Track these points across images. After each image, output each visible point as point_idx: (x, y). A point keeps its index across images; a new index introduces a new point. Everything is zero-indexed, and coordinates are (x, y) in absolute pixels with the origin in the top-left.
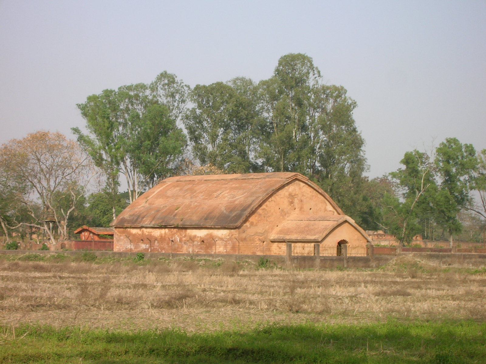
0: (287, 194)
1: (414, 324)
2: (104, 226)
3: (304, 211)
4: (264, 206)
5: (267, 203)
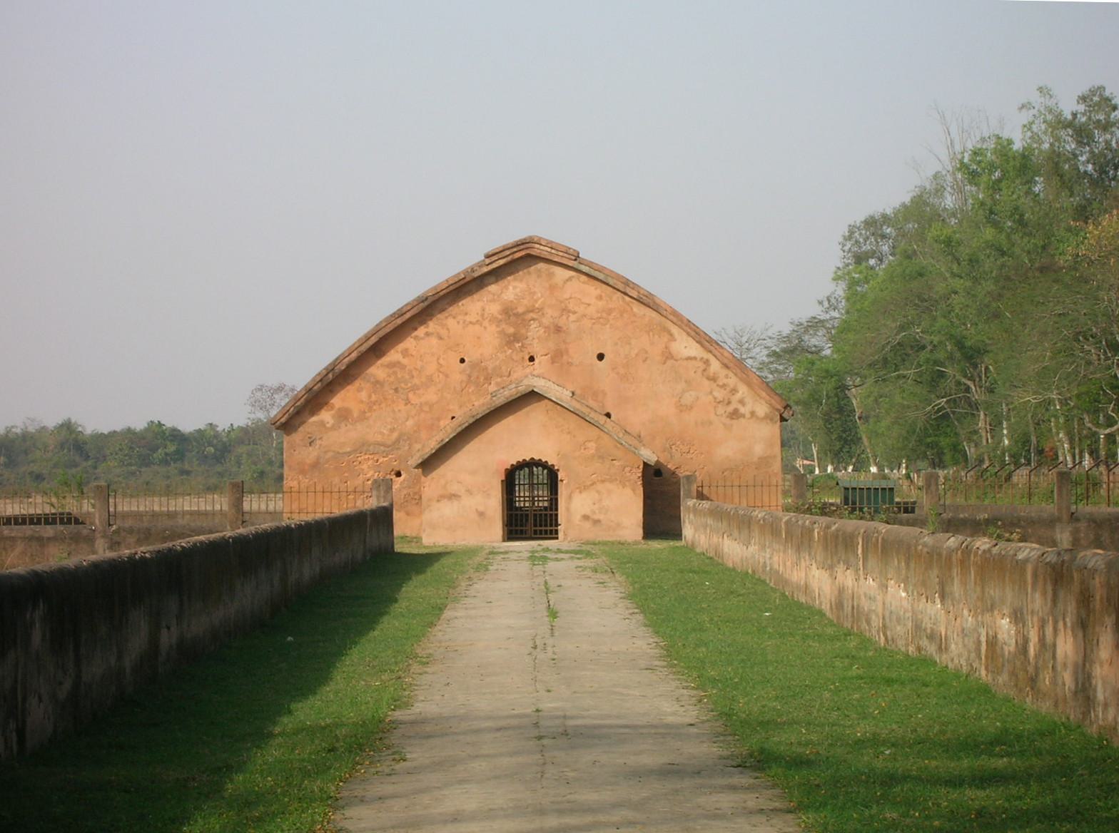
0: (494, 309)
3: (570, 364)
4: (393, 355)
5: (409, 343)
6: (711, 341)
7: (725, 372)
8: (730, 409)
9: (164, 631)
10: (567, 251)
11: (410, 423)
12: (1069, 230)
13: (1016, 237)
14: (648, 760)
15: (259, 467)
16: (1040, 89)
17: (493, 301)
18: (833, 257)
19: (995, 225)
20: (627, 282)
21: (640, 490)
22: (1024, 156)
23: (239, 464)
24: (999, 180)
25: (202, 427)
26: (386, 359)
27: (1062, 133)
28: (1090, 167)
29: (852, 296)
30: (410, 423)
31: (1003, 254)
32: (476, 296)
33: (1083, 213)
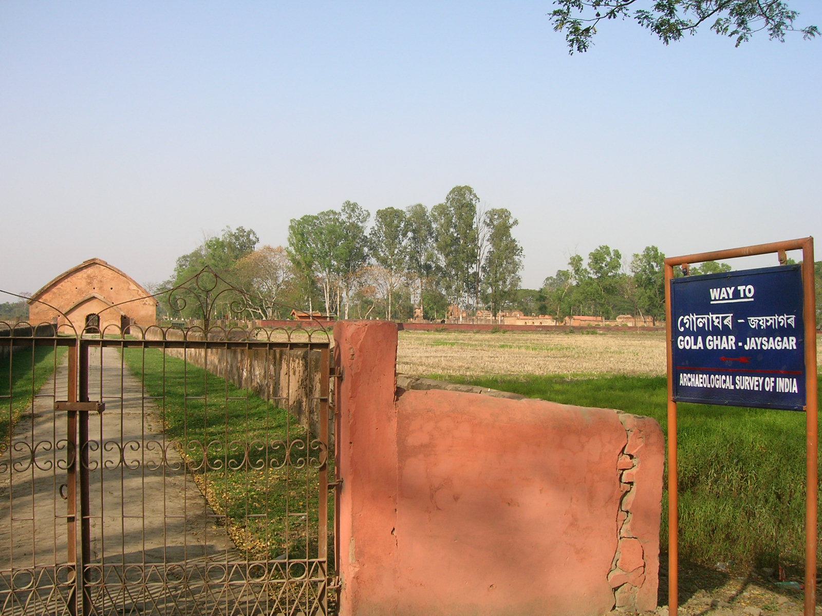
0: (85, 276)
1: (407, 340)
2: (680, 451)
3: (104, 290)
4: (59, 286)
5: (63, 283)
6: (139, 286)
7: (142, 293)
8: (144, 303)
9: (5, 349)
10: (104, 262)
11: (63, 303)
12: (233, 261)
13: (219, 263)
14: (116, 373)
15: (21, 314)
16: (227, 226)
17: (85, 274)
18: (175, 265)
19: (214, 259)
20: (119, 271)
21: (120, 322)
22: (222, 242)
23: (15, 313)
24: (216, 248)
25: (5, 303)
26: (57, 287)
27: (232, 237)
28: (239, 246)
29: (179, 275)
30: (63, 303)
31: (216, 266)
32: (80, 272)
33: (236, 257)
